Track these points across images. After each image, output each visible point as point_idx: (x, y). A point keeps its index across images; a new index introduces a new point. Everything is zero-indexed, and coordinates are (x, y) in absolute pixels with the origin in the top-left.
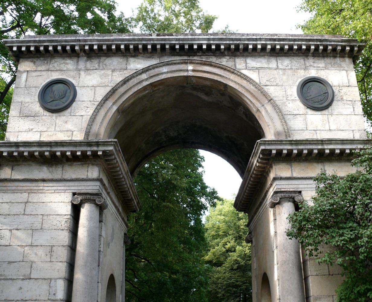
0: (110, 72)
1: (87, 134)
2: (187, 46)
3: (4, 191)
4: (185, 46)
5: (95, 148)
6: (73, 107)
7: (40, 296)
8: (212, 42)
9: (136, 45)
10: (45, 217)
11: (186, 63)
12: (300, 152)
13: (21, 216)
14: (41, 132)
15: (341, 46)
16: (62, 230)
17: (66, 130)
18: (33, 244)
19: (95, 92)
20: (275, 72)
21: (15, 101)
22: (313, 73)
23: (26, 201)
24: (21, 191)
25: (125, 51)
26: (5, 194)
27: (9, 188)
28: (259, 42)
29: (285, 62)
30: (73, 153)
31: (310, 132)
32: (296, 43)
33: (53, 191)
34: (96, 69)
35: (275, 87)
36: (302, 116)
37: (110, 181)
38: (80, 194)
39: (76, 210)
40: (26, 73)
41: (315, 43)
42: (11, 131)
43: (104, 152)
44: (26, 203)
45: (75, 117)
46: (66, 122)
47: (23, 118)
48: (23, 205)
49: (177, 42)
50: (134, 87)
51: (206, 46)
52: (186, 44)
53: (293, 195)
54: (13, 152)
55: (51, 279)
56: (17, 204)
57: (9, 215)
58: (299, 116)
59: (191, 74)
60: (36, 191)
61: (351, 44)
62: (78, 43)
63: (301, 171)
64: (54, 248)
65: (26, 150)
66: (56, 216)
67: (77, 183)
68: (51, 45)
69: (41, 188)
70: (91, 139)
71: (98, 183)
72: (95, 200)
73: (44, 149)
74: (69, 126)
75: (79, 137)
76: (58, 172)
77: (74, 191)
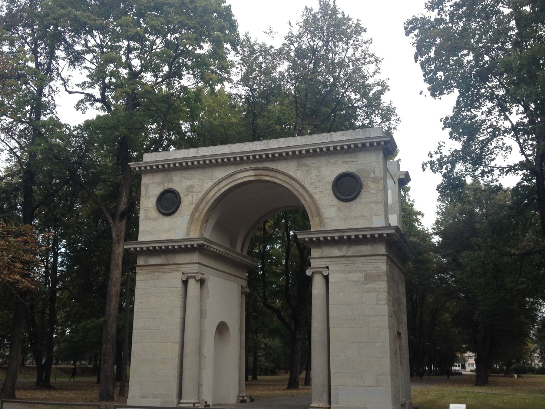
39: (185, 283)
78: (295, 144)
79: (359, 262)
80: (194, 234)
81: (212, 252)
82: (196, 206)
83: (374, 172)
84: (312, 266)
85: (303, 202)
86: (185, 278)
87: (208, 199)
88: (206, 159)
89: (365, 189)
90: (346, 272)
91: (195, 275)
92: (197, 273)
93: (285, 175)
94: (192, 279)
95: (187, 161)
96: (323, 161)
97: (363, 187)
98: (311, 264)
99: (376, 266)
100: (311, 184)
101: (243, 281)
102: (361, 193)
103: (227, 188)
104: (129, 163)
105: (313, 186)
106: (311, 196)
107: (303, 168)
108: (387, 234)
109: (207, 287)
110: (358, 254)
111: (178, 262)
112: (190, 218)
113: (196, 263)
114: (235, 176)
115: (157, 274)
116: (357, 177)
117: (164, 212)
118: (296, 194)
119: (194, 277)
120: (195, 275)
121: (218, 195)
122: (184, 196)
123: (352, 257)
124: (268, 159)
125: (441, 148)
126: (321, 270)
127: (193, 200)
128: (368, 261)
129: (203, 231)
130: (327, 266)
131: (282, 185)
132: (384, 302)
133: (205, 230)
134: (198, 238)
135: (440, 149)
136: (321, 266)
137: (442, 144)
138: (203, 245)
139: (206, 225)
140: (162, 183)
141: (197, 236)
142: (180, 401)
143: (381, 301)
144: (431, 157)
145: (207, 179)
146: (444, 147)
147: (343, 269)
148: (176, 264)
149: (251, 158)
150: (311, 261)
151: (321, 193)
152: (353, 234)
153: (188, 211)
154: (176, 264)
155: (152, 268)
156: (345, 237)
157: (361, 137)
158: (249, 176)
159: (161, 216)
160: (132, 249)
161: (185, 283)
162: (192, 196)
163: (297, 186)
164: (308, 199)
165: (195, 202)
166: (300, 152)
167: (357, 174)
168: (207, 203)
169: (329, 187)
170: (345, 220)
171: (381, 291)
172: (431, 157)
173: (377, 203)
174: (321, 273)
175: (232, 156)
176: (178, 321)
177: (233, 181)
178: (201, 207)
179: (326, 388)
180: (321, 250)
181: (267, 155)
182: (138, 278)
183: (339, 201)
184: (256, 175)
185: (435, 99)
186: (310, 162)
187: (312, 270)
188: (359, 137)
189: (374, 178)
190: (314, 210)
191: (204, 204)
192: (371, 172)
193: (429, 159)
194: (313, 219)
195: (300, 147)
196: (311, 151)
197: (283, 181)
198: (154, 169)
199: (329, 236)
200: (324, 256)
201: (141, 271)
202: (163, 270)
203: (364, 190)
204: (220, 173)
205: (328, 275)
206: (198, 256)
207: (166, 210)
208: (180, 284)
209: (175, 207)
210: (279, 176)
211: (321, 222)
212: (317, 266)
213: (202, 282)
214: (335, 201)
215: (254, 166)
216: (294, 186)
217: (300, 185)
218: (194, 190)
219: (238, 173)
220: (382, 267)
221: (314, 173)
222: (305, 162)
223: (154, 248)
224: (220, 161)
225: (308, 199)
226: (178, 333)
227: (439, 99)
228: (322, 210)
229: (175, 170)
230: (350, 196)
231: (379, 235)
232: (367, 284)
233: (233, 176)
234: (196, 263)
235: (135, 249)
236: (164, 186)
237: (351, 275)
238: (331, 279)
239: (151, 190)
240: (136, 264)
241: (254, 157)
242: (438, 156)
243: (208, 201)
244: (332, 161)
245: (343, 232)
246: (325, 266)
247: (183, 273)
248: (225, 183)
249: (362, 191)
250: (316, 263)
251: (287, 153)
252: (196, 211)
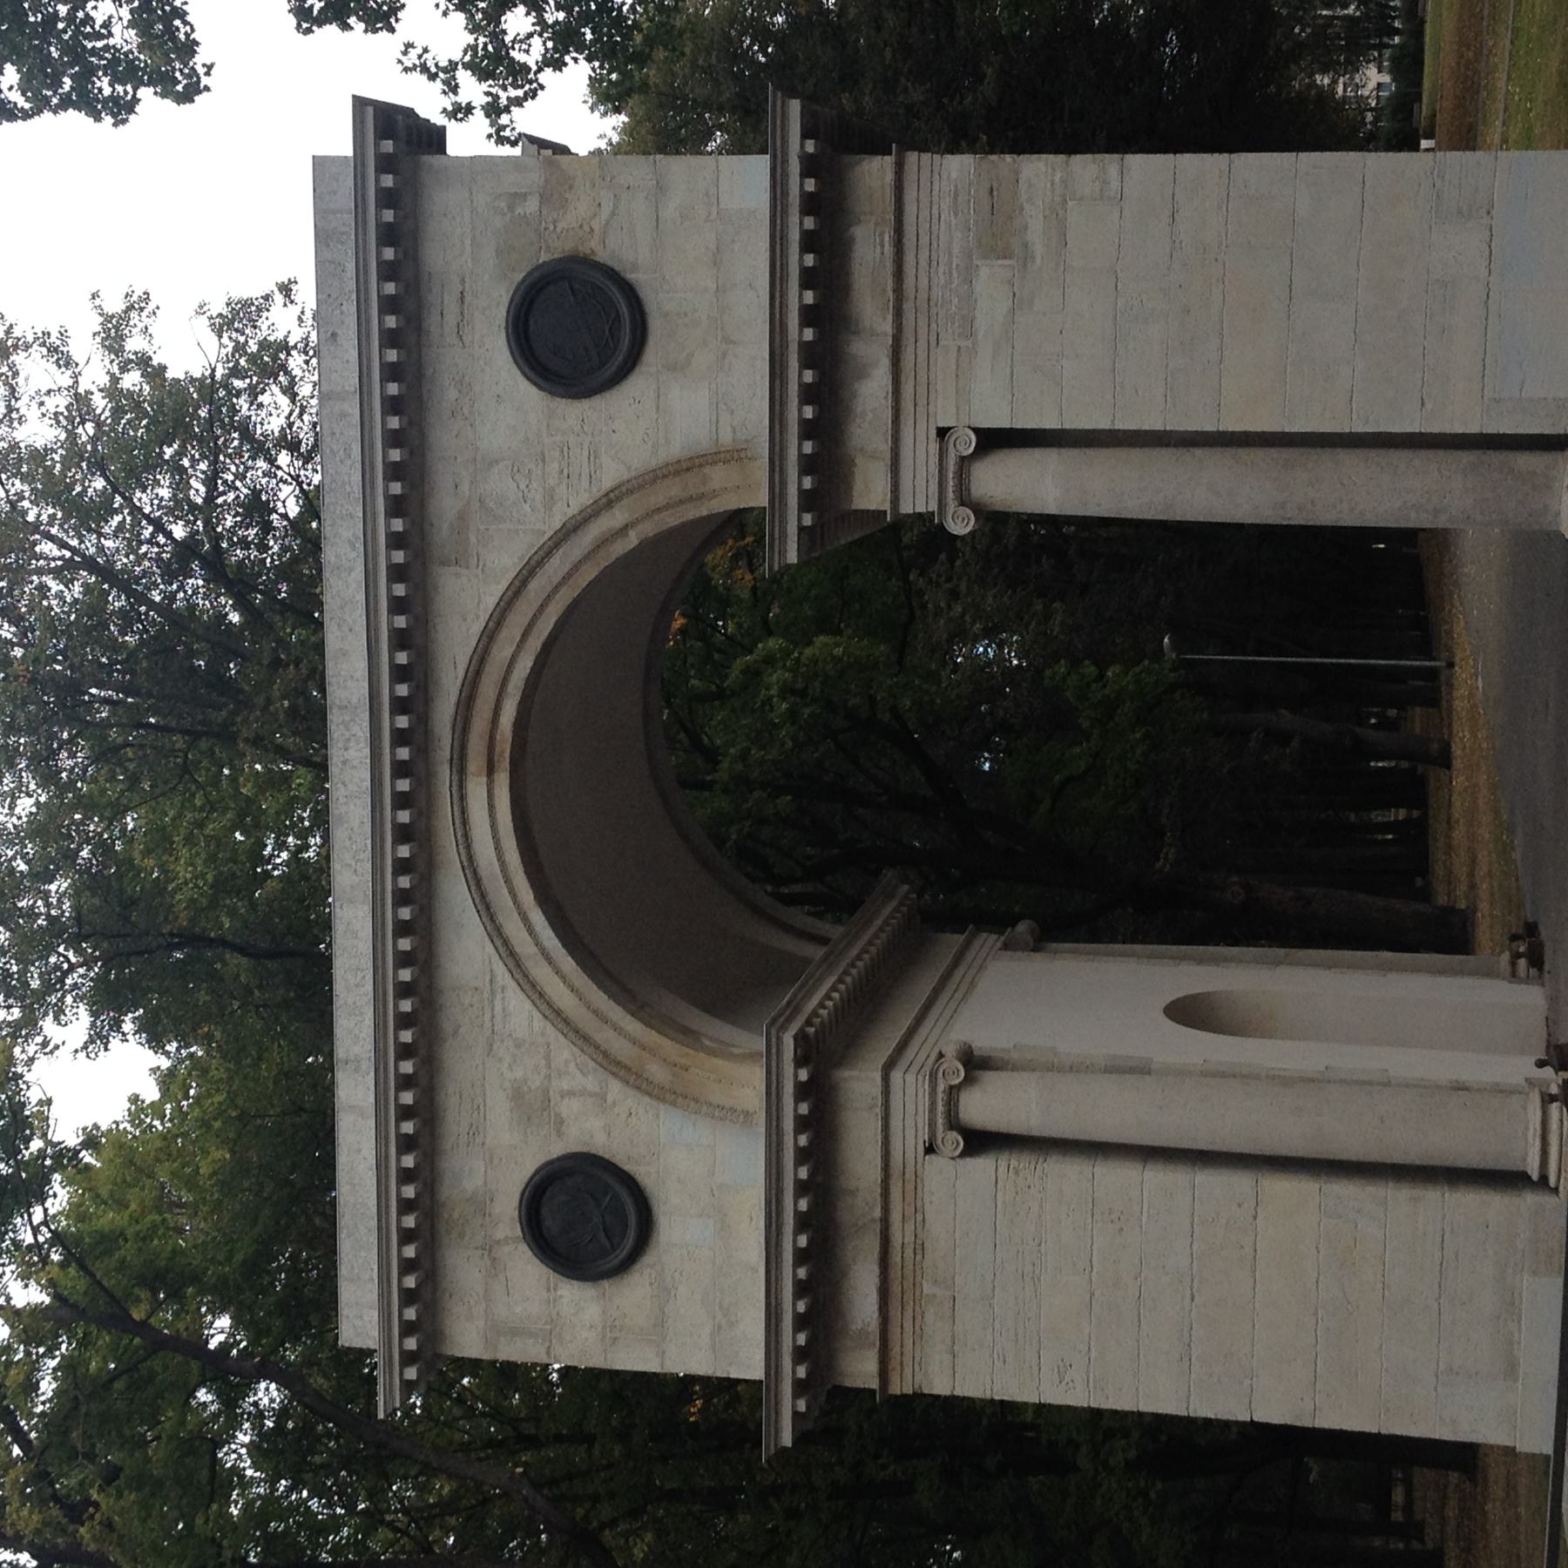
39: (979, 1142)
77: (921, 1149)
78: (360, 568)
79: (923, 282)
80: (749, 1085)
81: (840, 1012)
82: (614, 1075)
83: (518, 197)
84: (933, 507)
85: (633, 540)
86: (954, 1141)
87: (584, 1010)
89: (594, 244)
90: (969, 343)
91: (941, 1087)
92: (933, 1076)
93: (499, 624)
94: (961, 1108)
96: (446, 440)
97: (584, 249)
98: (921, 509)
99: (946, 204)
100: (550, 498)
101: (977, 944)
102: (610, 263)
103: (538, 918)
104: (381, 1416)
105: (562, 490)
106: (608, 502)
107: (473, 539)
108: (805, 135)
109: (1004, 1050)
110: (890, 284)
111: (876, 1175)
112: (673, 1104)
113: (886, 1079)
114: (483, 872)
115: (927, 1288)
116: (536, 274)
117: (629, 1242)
118: (589, 573)
119: (953, 1092)
120: (941, 1087)
121: (568, 963)
122: (560, 1134)
123: (898, 314)
124: (416, 737)
125: (431, 64)
126: (941, 1097)
127: (583, 1093)
128: (924, 240)
129: (736, 1051)
131: (545, 899)
132: (1113, 171)
133: (733, 1046)
134: (768, 1072)
135: (433, 70)
136: (934, 460)
137: (412, 58)
138: (801, 1038)
139: (711, 1039)
140: (489, 1248)
141: (756, 1076)
142: (1535, 1177)
143: (1105, 182)
144: (469, 109)
145: (488, 1016)
146: (426, 50)
147: (953, 356)
149: (404, 785)
150: (906, 508)
151: (594, 455)
152: (798, 297)
153: (634, 1120)
155: (895, 1313)
156: (810, 185)
157: (351, 253)
158: (491, 807)
159: (648, 1259)
160: (802, 1406)
161: (979, 1142)
162: (564, 1095)
163: (557, 566)
164: (616, 518)
165: (591, 1080)
166: (396, 541)
167: (519, 276)
168: (605, 1021)
169: (573, 412)
170: (727, 340)
171: (1064, 181)
172: (469, 109)
173: (661, 188)
174: (964, 461)
175: (387, 750)
176: (1157, 1177)
177: (508, 880)
178: (621, 1048)
179: (1496, 458)
180: (859, 460)
181: (400, 706)
182: (940, 1386)
183: (637, 370)
184: (491, 770)
185: (207, 89)
186: (445, 504)
187: (952, 505)
188: (351, 266)
189: (544, 198)
190: (673, 489)
191: (604, 1036)
192: (519, 210)
193: (479, 114)
194: (714, 494)
195: (375, 539)
196: (396, 488)
197: (525, 635)
198: (419, 1285)
199: (798, 412)
200: (885, 447)
201: (908, 1371)
202: (909, 1252)
203: (598, 249)
205: (976, 431)
206: (855, 1073)
207: (623, 1236)
208: (983, 1165)
209: (611, 1181)
210: (502, 651)
211: (735, 456)
212: (934, 487)
213: (975, 1064)
214: (637, 386)
215: (444, 775)
216: (556, 580)
217: (549, 554)
218: (536, 1082)
219: (470, 858)
220: (954, 175)
221: (499, 484)
222: (445, 526)
223: (801, 1289)
224: (405, 944)
225: (616, 518)
226: (1211, 1181)
227: (208, 74)
228: (675, 449)
229: (433, 1181)
230: (618, 316)
231: (804, 507)
232: (1026, 245)
233: (485, 881)
234: (886, 1079)
235: (800, 1387)
236: (506, 1240)
237: (981, 324)
238: (999, 419)
239: (518, 1310)
240: (873, 1392)
241: (400, 770)
242: (464, 77)
243: (596, 1012)
244: (452, 394)
245: (784, 345)
246: (934, 447)
247: (930, 1149)
248: (513, 928)
249: (602, 256)
250: (920, 483)
251: (398, 606)
252: (639, 1076)
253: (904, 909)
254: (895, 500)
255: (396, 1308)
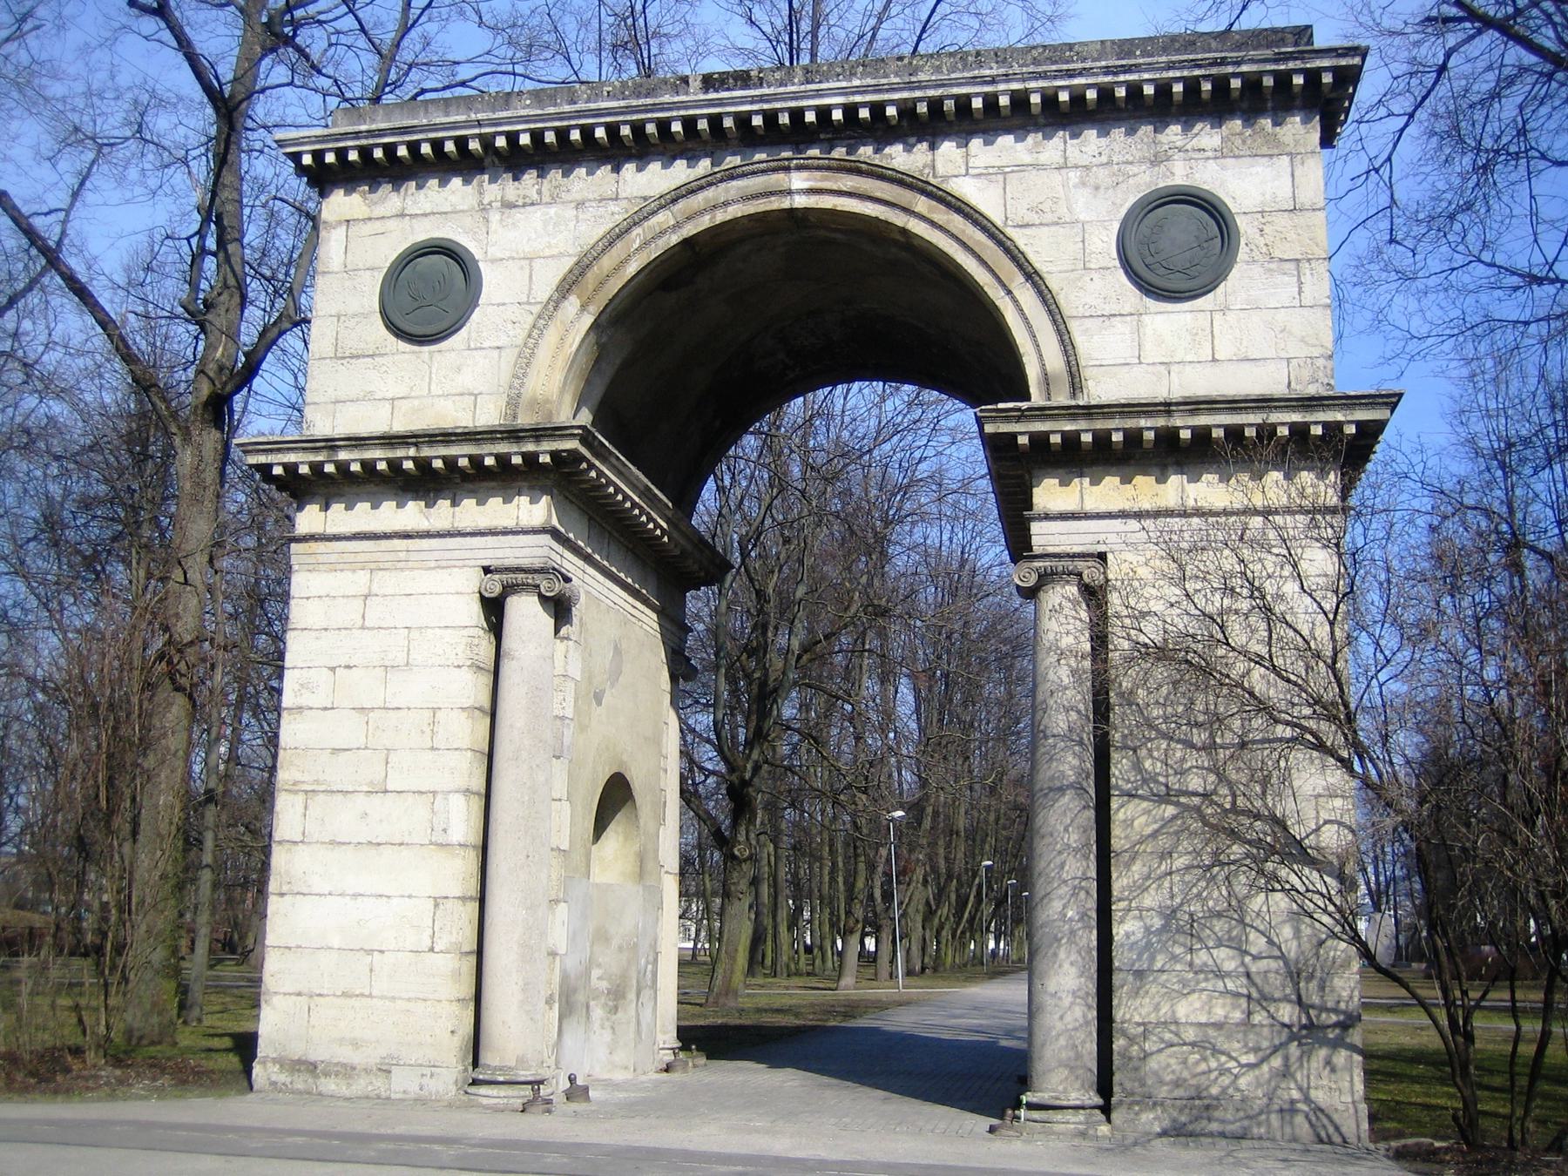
0: (570, 212)
1: (513, 403)
2: (787, 115)
3: (311, 567)
4: (973, 100)
5: (530, 447)
6: (474, 325)
7: (410, 834)
8: (858, 99)
9: (1050, 92)
10: (414, 634)
11: (787, 169)
12: (1102, 439)
13: (357, 633)
14: (393, 399)
15: (1274, 73)
16: (459, 666)
17: (458, 391)
18: (387, 705)
19: (531, 277)
20: (1056, 177)
21: (320, 313)
22: (1179, 175)
23: (366, 592)
24: (354, 567)
25: (1126, 103)
26: (315, 574)
27: (321, 559)
28: (1002, 87)
29: (1090, 143)
30: (476, 461)
31: (1151, 368)
32: (1122, 78)
33: (433, 564)
34: (532, 204)
35: (1053, 228)
36: (1128, 318)
37: (615, 534)
38: (498, 570)
39: (494, 610)
40: (344, 227)
41: (1186, 73)
42: (316, 400)
43: (555, 455)
44: (366, 597)
45: (480, 352)
46: (459, 370)
47: (345, 362)
48: (360, 601)
49: (755, 107)
50: (634, 258)
51: (1331, 75)
52: (782, 110)
53: (1080, 565)
54: (322, 464)
55: (434, 793)
56: (345, 600)
57: (326, 629)
58: (1119, 318)
59: (800, 202)
60: (387, 565)
61: (1308, 66)
62: (477, 131)
63: (1111, 493)
64: (439, 714)
65: (352, 458)
66: (442, 631)
67: (490, 541)
68: (402, 143)
69: (402, 555)
70: (525, 420)
71: (546, 539)
72: (538, 586)
73: (400, 453)
74: (467, 380)
75: (489, 415)
76: (443, 514)
77: (486, 563)
88: (698, 112)
95: (565, 123)
130: (1102, 548)
148: (1139, 515)
150: (1035, 527)
154: (1139, 515)
182: (301, 583)
200: (331, 530)
204: (656, 178)
208: (473, 613)
213: (560, 608)
253: (658, 532)
254: (1047, 517)
255: (628, 118)
